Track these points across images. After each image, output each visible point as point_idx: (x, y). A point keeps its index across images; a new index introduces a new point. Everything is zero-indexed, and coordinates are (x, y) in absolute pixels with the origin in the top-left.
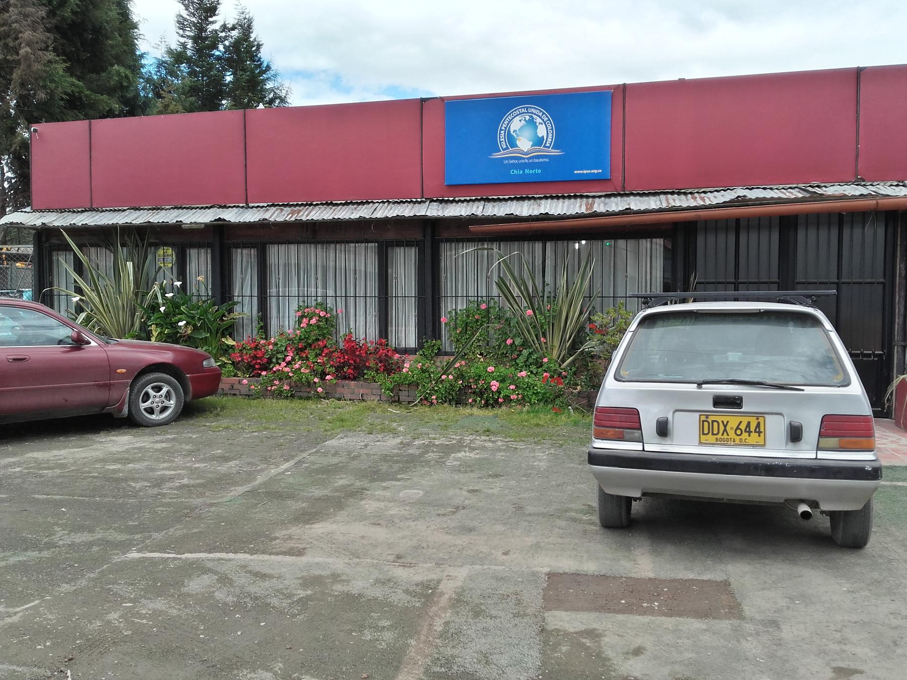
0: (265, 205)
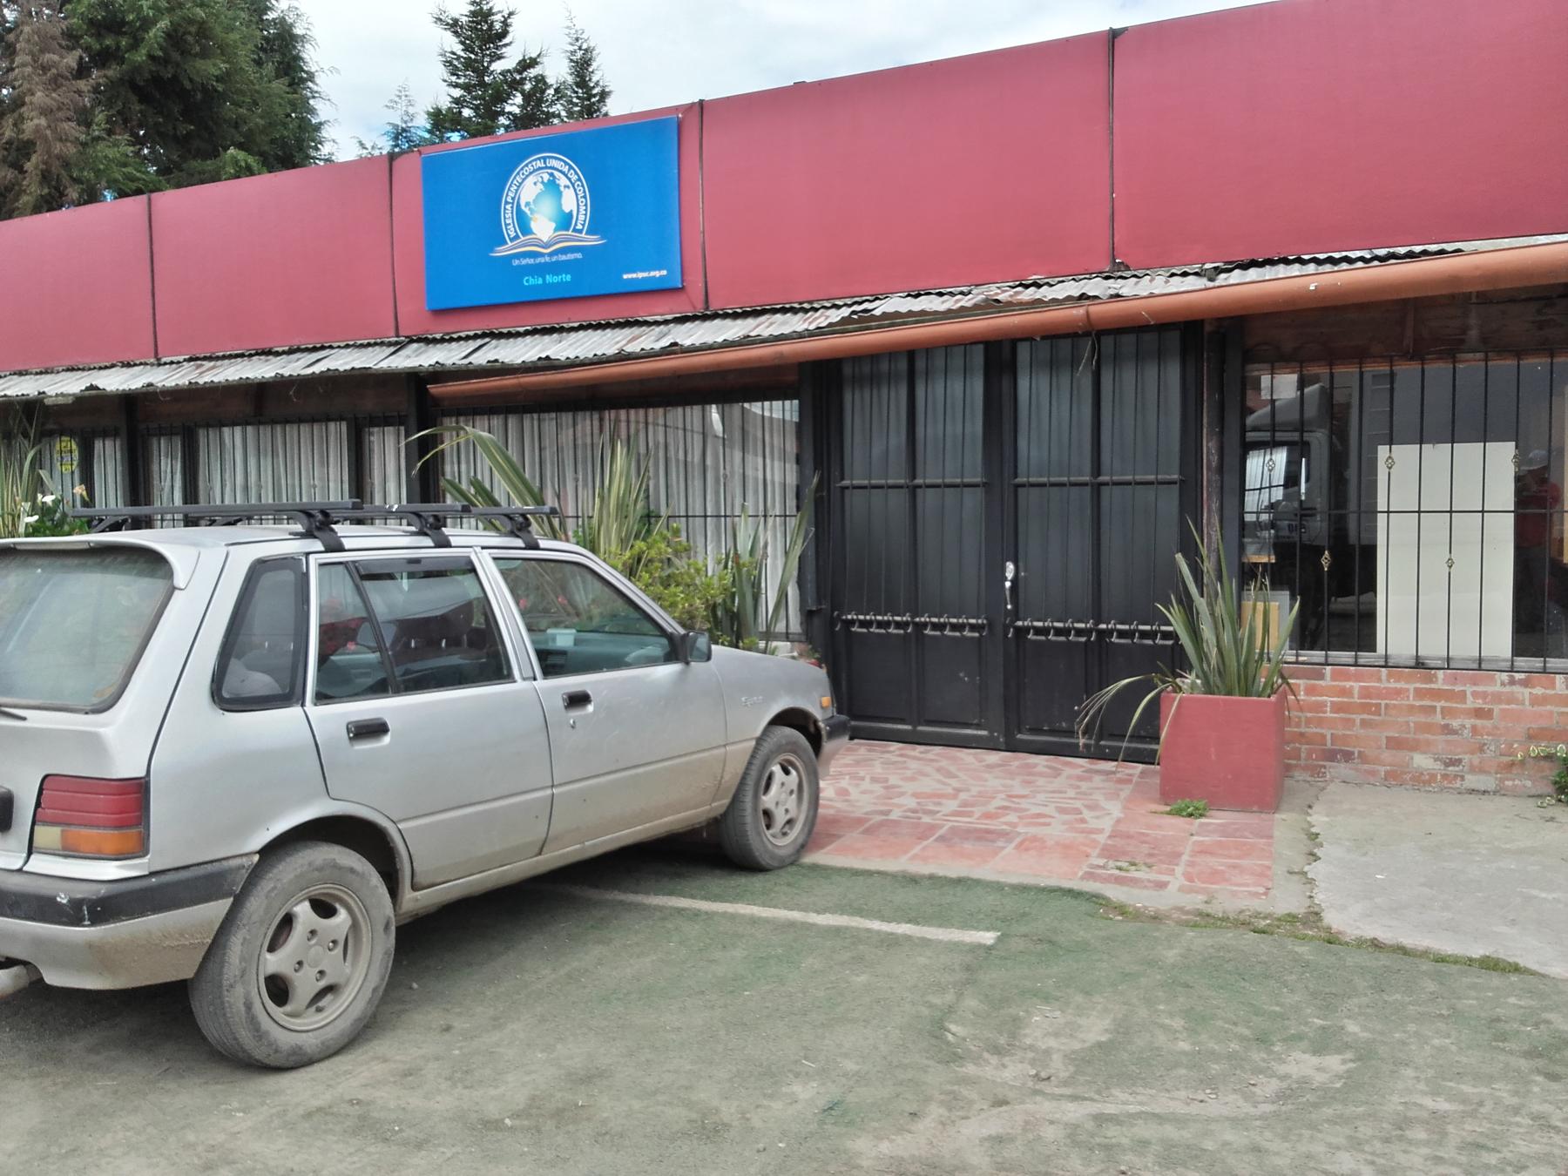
0: (181, 358)
